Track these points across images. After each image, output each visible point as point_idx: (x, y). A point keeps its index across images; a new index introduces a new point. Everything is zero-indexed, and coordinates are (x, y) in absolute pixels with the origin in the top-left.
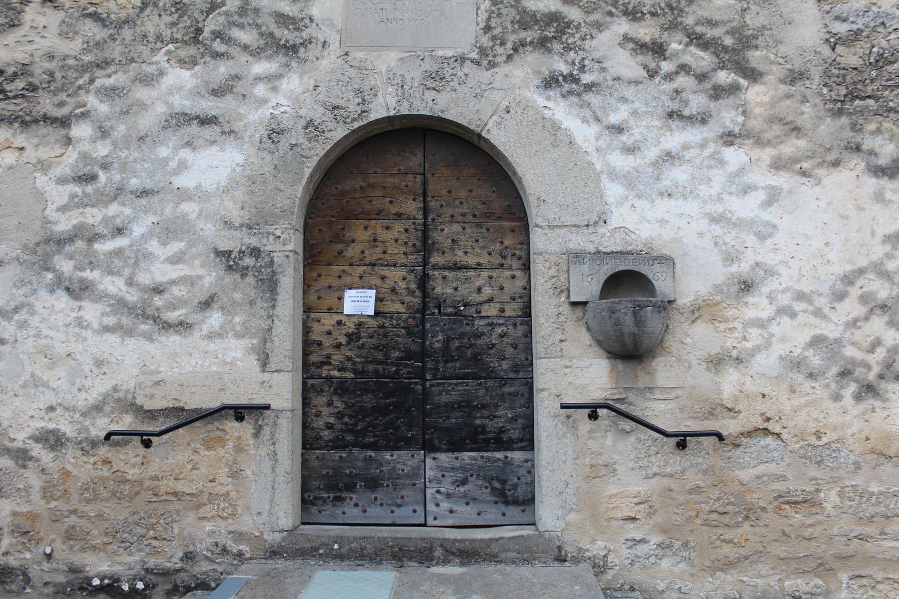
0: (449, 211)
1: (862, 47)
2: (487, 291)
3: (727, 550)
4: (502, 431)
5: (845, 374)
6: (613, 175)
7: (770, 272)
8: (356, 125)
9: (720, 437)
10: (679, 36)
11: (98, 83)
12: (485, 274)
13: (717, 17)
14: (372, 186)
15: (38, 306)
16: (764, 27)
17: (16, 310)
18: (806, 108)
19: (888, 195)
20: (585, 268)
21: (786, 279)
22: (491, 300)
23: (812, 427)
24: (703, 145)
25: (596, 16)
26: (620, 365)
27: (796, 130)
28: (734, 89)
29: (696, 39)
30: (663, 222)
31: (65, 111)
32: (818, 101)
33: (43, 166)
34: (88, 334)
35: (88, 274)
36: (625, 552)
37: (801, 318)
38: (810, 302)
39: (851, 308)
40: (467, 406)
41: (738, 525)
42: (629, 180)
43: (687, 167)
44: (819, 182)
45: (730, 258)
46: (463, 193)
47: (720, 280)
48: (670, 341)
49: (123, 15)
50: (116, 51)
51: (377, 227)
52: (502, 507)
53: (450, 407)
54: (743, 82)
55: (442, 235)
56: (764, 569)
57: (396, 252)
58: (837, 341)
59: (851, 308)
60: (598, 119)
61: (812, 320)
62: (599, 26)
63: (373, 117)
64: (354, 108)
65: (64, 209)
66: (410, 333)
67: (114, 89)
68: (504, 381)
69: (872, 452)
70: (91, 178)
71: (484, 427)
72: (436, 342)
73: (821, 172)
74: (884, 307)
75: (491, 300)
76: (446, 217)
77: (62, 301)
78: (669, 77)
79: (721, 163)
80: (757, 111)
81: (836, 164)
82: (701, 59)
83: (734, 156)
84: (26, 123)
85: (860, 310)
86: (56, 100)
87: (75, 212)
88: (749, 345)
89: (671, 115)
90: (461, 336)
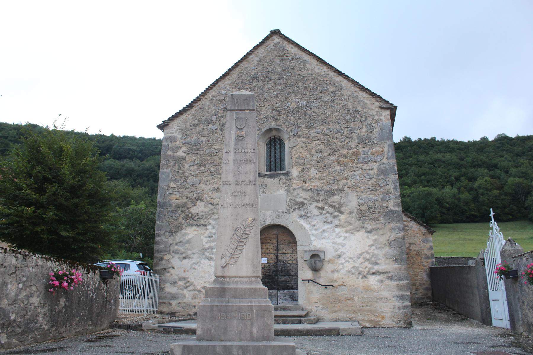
0: (282, 242)
1: (366, 205)
2: (290, 258)
3: (335, 308)
4: (293, 286)
5: (359, 273)
6: (313, 235)
7: (344, 253)
8: (263, 226)
9: (333, 286)
10: (327, 205)
11: (212, 217)
12: (289, 255)
13: (335, 201)
14: (267, 237)
15: (202, 262)
16: (345, 203)
17: (198, 263)
18: (353, 219)
19: (370, 237)
20: (307, 253)
21: (348, 255)
22: (290, 260)
23: (352, 284)
24: (331, 228)
25: (310, 202)
26: (314, 272)
27: (351, 224)
28: (338, 216)
29: (331, 206)
30: (323, 244)
31: (206, 223)
32: (355, 218)
33: (202, 234)
34: (212, 267)
35: (212, 256)
36: (315, 309)
37: (350, 262)
38: (352, 259)
39: (361, 260)
40: (286, 281)
41: (337, 304)
42: (316, 236)
43: (328, 233)
44: (355, 235)
45: (336, 251)
46: (285, 238)
47: (334, 255)
48: (324, 267)
49: (216, 203)
50: (215, 211)
51: (268, 246)
52: (293, 301)
53: (282, 281)
54: (340, 214)
55: (280, 247)
56: (343, 312)
57: (272, 251)
58: (358, 267)
59: (361, 260)
60: (310, 224)
61: (353, 263)
62: (311, 204)
63: (266, 224)
64: (263, 223)
65: (206, 243)
66: (274, 267)
67: (215, 219)
68: (293, 276)
69: (365, 289)
70: (212, 237)
71: (289, 286)
72: (280, 269)
73: (355, 233)
74: (368, 260)
75: (290, 260)
76: (281, 243)
77: (207, 261)
78: (325, 214)
79: (335, 231)
80: (343, 220)
81: (359, 231)
82: (331, 210)
83: (338, 230)
84: (198, 226)
85: (363, 261)
86: (204, 221)
87: (209, 244)
88: (340, 268)
89: (325, 222)
90: (285, 267)
